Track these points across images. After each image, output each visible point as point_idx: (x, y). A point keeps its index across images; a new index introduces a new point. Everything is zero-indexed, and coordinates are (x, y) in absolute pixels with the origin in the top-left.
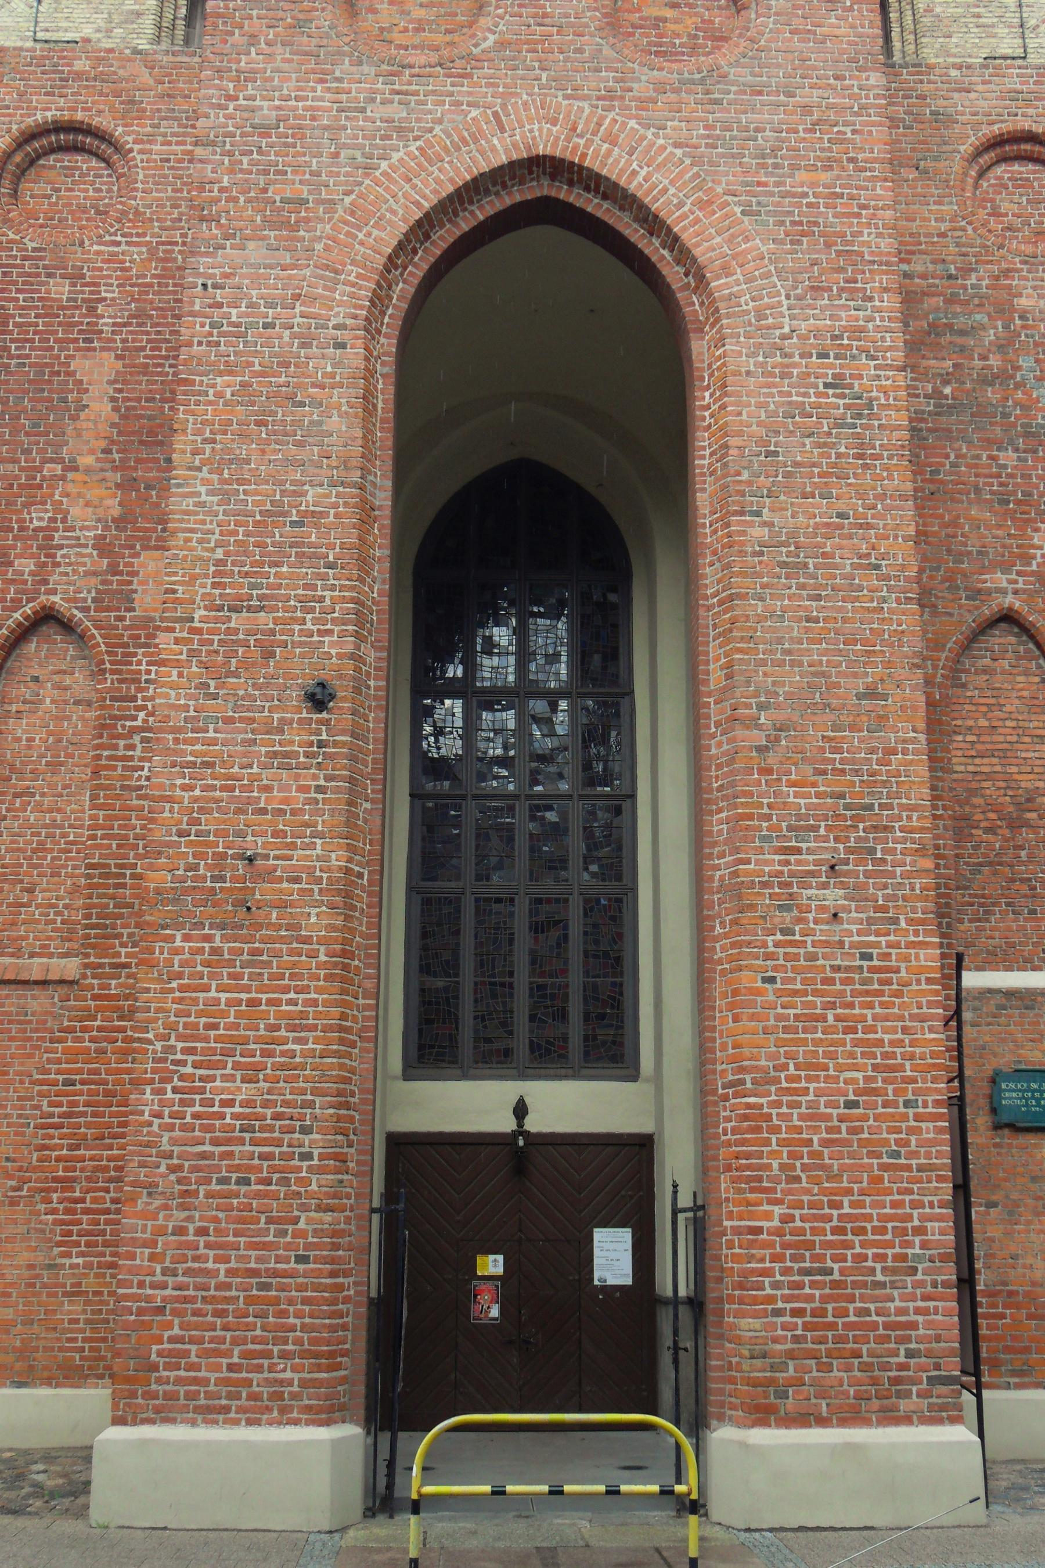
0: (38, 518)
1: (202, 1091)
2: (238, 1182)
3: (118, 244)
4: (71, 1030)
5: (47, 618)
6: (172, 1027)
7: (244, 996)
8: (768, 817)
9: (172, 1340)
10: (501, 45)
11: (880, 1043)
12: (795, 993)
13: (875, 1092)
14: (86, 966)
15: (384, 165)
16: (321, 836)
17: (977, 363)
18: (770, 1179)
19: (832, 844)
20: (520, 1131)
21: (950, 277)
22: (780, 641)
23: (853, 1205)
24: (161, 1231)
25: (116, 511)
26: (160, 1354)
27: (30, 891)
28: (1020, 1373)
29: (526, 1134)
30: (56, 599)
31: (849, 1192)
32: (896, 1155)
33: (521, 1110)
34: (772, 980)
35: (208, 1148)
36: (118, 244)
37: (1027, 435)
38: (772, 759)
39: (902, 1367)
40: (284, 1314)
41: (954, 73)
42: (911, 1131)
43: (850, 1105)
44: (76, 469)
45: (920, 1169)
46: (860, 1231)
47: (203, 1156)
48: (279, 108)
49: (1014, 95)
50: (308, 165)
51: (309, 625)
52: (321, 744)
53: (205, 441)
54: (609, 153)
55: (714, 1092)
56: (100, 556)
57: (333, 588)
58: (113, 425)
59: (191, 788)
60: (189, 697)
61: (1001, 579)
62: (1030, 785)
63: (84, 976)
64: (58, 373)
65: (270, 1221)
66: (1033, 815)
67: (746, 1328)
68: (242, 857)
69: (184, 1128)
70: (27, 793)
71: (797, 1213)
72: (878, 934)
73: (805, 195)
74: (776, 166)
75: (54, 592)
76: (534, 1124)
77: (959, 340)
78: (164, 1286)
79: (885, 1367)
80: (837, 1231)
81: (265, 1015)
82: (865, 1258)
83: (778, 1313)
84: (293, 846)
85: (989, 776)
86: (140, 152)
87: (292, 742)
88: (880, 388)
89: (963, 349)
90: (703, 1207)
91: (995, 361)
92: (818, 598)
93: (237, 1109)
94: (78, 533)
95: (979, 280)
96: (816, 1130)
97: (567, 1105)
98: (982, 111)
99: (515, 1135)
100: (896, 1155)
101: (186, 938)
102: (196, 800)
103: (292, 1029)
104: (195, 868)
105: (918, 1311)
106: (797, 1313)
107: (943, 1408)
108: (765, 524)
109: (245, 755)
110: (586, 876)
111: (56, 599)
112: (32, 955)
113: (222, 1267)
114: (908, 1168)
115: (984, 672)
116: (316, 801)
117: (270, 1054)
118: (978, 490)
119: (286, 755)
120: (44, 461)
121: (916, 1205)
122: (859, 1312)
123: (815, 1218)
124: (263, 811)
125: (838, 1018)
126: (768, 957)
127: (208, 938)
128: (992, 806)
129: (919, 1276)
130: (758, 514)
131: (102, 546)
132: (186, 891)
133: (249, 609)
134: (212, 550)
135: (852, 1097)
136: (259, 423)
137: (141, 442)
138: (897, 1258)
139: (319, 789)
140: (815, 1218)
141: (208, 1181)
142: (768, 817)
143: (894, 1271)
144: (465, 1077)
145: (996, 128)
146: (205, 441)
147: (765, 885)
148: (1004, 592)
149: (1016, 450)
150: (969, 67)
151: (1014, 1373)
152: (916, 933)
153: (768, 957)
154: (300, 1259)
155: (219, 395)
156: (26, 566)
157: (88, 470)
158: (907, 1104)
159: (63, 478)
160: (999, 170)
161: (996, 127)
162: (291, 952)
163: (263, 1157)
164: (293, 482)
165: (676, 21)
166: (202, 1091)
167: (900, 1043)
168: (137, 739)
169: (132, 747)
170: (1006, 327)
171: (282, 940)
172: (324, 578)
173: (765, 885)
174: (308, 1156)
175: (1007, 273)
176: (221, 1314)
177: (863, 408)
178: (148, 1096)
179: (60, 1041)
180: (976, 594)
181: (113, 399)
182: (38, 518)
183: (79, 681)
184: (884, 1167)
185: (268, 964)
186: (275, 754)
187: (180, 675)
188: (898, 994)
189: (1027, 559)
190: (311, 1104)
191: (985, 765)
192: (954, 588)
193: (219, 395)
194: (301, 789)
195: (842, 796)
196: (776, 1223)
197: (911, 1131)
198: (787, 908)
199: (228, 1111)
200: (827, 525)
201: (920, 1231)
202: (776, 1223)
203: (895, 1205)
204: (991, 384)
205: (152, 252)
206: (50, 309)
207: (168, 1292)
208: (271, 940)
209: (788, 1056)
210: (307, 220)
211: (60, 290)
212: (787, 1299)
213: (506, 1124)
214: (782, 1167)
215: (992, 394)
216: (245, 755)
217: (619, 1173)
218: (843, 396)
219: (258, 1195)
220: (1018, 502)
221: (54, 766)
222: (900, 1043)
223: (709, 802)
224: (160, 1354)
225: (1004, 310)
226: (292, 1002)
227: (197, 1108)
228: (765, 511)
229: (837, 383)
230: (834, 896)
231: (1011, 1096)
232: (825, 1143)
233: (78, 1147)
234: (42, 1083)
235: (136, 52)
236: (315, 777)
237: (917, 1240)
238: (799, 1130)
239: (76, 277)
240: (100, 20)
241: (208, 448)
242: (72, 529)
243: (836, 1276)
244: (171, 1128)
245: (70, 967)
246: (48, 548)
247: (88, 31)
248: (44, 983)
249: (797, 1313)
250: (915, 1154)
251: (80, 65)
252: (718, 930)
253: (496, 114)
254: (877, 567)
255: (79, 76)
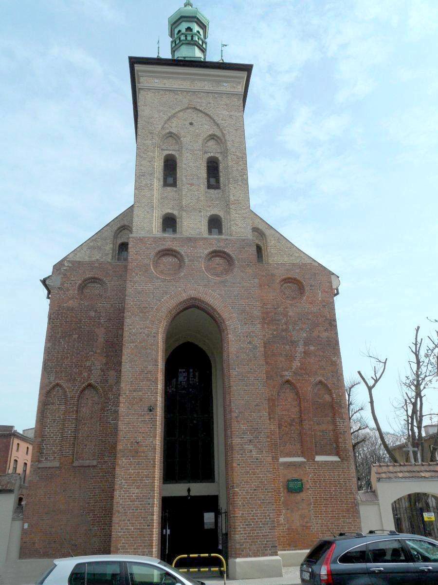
0: (88, 364)
1: (128, 491)
2: (136, 510)
3: (105, 304)
4: (94, 476)
5: (90, 385)
6: (122, 478)
7: (137, 471)
8: (238, 431)
9: (123, 543)
10: (185, 275)
11: (260, 477)
12: (244, 467)
13: (260, 487)
14: (99, 462)
15: (163, 300)
16: (151, 437)
17: (281, 327)
18: (239, 506)
19: (250, 436)
20: (189, 495)
21: (275, 309)
22: (240, 395)
23: (256, 511)
24: (120, 521)
25: (105, 362)
26: (120, 546)
27: (86, 446)
28: (295, 547)
29: (191, 496)
30: (92, 381)
31: (254, 508)
32: (263, 500)
33: (189, 490)
34: (239, 465)
35: (130, 503)
36: (105, 304)
37: (291, 342)
38: (239, 419)
39: (266, 544)
40: (145, 537)
41: (275, 265)
42: (267, 495)
43: (255, 490)
44: (96, 353)
45: (269, 503)
46: (257, 516)
47: (129, 504)
48: (142, 288)
49: (287, 270)
50: (147, 300)
51: (149, 394)
52: (151, 419)
53: (129, 357)
54: (206, 296)
55: (228, 488)
56: (101, 372)
57: (154, 386)
58: (104, 343)
59: (126, 428)
60: (125, 409)
61: (287, 373)
62: (294, 417)
63: (98, 464)
64: (92, 332)
65: (142, 518)
66: (295, 423)
67: (239, 536)
68: (136, 442)
69: (125, 499)
70: (85, 424)
71: (244, 512)
72: (259, 454)
73: (243, 304)
74: (238, 299)
75: (91, 380)
76: (192, 494)
77: (277, 322)
78: (120, 532)
79: (262, 544)
80: (253, 516)
81: (141, 475)
82: (258, 522)
83: (242, 534)
84: (146, 440)
85: (285, 415)
86: (109, 284)
87: (146, 418)
88: (258, 344)
89: (278, 324)
90: (226, 512)
91: (284, 327)
92: (247, 386)
93: (135, 495)
94: (97, 367)
95: (281, 309)
96: (248, 495)
97: (199, 489)
98: (281, 274)
99: (188, 496)
100: (263, 500)
101: (126, 459)
102: (127, 430)
103: (146, 477)
104: (127, 445)
105: (269, 532)
106: (245, 534)
107: (274, 552)
108: (236, 371)
109: (137, 421)
110: (202, 435)
111: (92, 381)
112: (86, 460)
113: (133, 528)
114: (266, 503)
115: (284, 392)
116: (150, 430)
117: (142, 483)
118: (281, 354)
119: (145, 421)
120: (89, 351)
121: (267, 510)
122: (257, 533)
123: (248, 514)
124: (140, 433)
125: (252, 472)
126: (238, 460)
127: (130, 459)
128: (286, 421)
129: (269, 525)
130: (235, 369)
131: (102, 370)
132: (125, 449)
133: (137, 391)
134: (130, 379)
135: (255, 488)
136: (139, 353)
137: (110, 347)
138: (265, 521)
139: (151, 428)
140: (248, 514)
141: (130, 510)
142: (238, 431)
143: (264, 524)
144: (177, 482)
145: (284, 277)
146: (129, 357)
147: (238, 445)
148: (287, 376)
149: (289, 345)
150: (278, 264)
151: (294, 547)
152: (267, 454)
153: (238, 460)
154: (148, 526)
155: (131, 347)
156: (85, 374)
157: (99, 353)
158: (266, 489)
159: (93, 355)
160: (285, 285)
161: (284, 277)
162: (146, 462)
163: (140, 504)
164: (146, 365)
165: (218, 268)
166: (128, 491)
167: (264, 477)
168: (109, 411)
169: (108, 413)
170: (286, 319)
171: (144, 459)
172: (152, 384)
173: (238, 445)
174: (149, 504)
175: (286, 308)
176: (132, 537)
177: (255, 347)
178: (118, 492)
179: (92, 479)
180: (282, 376)
181: (104, 338)
182: (88, 364)
183: (96, 398)
184: (261, 503)
185: (141, 464)
186: (143, 421)
187: (124, 405)
188: (263, 467)
189: (292, 368)
190: (150, 493)
191: (284, 413)
192: (277, 375)
193: (131, 347)
194: (147, 428)
195: (252, 426)
196: (241, 515)
197: (267, 495)
198: (242, 450)
199: (134, 495)
200: (248, 371)
201: (269, 515)
202: (241, 515)
203: (264, 510)
204: (283, 331)
205: (112, 305)
206: (90, 318)
207: (122, 533)
208: (142, 459)
209: (243, 480)
210: (148, 311)
211: (92, 314)
212: (243, 531)
213: (186, 494)
214: (242, 503)
215: (284, 333)
216: (137, 421)
217: (211, 503)
218: (251, 345)
219: (140, 512)
220: (290, 357)
221: (92, 418)
222: (264, 477)
223: (227, 427)
224: (120, 546)
225: (286, 315)
226: (147, 472)
227: (128, 495)
228: (236, 369)
229: (250, 343)
230: (251, 447)
231: (291, 485)
232: (250, 498)
233: (96, 502)
234: (89, 488)
235: (108, 262)
236: (150, 425)
237: (268, 517)
238: (245, 495)
239: (96, 311)
240: (100, 255)
241: (129, 358)
242: (96, 366)
243: (253, 526)
244: (122, 499)
245: (95, 463)
246: (90, 370)
247: (98, 257)
248: (89, 466)
249: (245, 534)
250: (267, 500)
251: (96, 265)
252: (229, 454)
253: (184, 289)
254: (258, 380)
255: (96, 267)
